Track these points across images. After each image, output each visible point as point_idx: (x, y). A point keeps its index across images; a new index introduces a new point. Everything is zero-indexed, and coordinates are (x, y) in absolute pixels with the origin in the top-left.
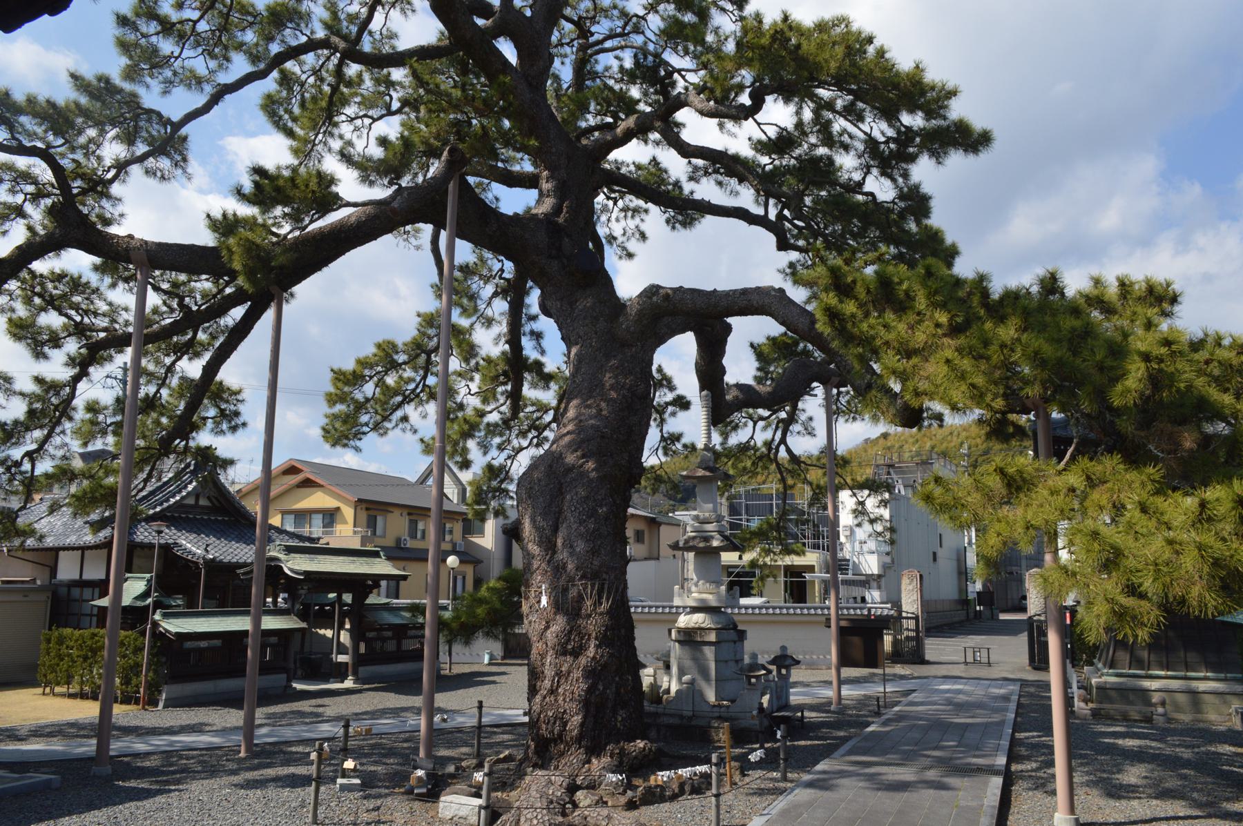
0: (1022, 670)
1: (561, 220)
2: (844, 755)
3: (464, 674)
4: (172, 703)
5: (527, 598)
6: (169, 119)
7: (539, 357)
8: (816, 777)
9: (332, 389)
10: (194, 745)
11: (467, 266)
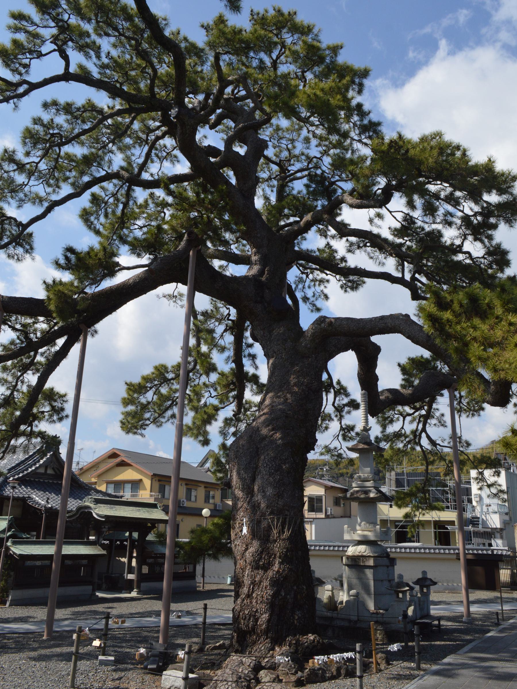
2: (466, 652)
3: (212, 590)
4: (15, 603)
5: (234, 528)
6: (21, 222)
7: (255, 372)
8: (442, 667)
9: (126, 396)
10: (17, 630)
11: (206, 312)
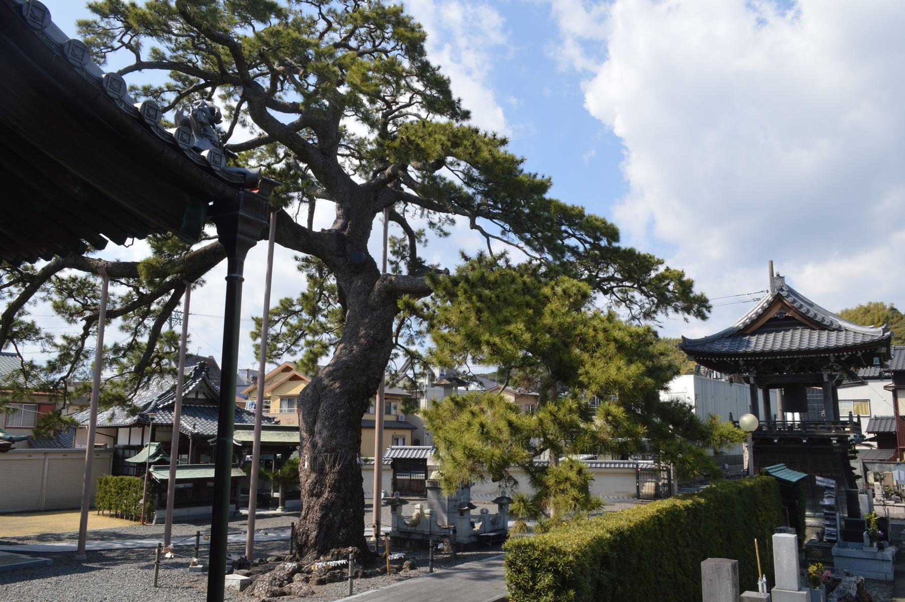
1: (346, 233)
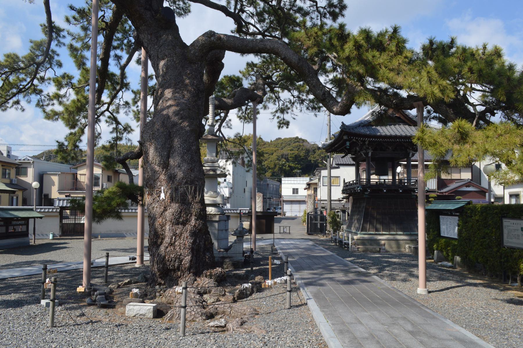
0: (304, 235)
3: (43, 245)
